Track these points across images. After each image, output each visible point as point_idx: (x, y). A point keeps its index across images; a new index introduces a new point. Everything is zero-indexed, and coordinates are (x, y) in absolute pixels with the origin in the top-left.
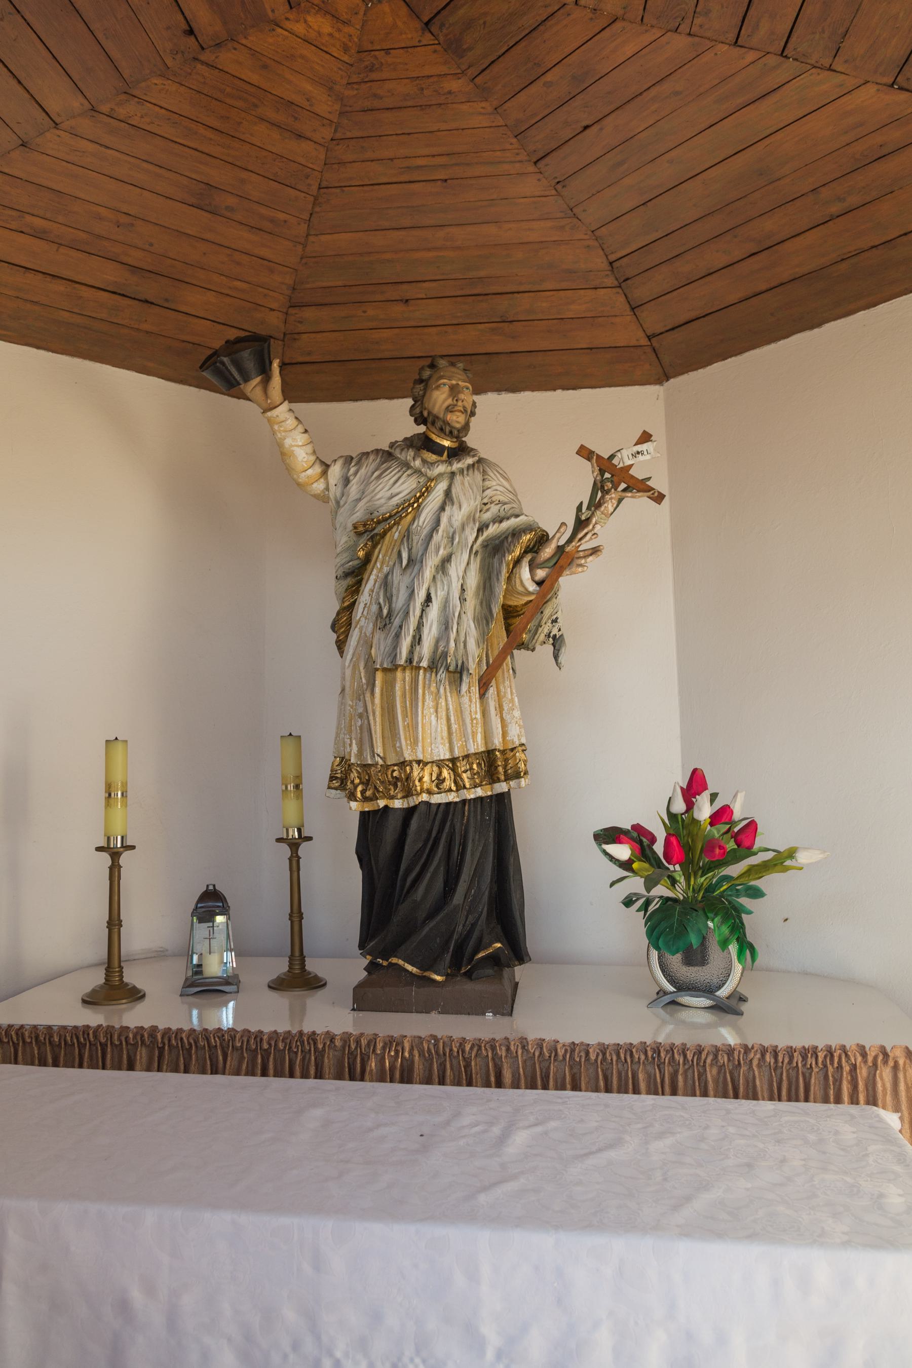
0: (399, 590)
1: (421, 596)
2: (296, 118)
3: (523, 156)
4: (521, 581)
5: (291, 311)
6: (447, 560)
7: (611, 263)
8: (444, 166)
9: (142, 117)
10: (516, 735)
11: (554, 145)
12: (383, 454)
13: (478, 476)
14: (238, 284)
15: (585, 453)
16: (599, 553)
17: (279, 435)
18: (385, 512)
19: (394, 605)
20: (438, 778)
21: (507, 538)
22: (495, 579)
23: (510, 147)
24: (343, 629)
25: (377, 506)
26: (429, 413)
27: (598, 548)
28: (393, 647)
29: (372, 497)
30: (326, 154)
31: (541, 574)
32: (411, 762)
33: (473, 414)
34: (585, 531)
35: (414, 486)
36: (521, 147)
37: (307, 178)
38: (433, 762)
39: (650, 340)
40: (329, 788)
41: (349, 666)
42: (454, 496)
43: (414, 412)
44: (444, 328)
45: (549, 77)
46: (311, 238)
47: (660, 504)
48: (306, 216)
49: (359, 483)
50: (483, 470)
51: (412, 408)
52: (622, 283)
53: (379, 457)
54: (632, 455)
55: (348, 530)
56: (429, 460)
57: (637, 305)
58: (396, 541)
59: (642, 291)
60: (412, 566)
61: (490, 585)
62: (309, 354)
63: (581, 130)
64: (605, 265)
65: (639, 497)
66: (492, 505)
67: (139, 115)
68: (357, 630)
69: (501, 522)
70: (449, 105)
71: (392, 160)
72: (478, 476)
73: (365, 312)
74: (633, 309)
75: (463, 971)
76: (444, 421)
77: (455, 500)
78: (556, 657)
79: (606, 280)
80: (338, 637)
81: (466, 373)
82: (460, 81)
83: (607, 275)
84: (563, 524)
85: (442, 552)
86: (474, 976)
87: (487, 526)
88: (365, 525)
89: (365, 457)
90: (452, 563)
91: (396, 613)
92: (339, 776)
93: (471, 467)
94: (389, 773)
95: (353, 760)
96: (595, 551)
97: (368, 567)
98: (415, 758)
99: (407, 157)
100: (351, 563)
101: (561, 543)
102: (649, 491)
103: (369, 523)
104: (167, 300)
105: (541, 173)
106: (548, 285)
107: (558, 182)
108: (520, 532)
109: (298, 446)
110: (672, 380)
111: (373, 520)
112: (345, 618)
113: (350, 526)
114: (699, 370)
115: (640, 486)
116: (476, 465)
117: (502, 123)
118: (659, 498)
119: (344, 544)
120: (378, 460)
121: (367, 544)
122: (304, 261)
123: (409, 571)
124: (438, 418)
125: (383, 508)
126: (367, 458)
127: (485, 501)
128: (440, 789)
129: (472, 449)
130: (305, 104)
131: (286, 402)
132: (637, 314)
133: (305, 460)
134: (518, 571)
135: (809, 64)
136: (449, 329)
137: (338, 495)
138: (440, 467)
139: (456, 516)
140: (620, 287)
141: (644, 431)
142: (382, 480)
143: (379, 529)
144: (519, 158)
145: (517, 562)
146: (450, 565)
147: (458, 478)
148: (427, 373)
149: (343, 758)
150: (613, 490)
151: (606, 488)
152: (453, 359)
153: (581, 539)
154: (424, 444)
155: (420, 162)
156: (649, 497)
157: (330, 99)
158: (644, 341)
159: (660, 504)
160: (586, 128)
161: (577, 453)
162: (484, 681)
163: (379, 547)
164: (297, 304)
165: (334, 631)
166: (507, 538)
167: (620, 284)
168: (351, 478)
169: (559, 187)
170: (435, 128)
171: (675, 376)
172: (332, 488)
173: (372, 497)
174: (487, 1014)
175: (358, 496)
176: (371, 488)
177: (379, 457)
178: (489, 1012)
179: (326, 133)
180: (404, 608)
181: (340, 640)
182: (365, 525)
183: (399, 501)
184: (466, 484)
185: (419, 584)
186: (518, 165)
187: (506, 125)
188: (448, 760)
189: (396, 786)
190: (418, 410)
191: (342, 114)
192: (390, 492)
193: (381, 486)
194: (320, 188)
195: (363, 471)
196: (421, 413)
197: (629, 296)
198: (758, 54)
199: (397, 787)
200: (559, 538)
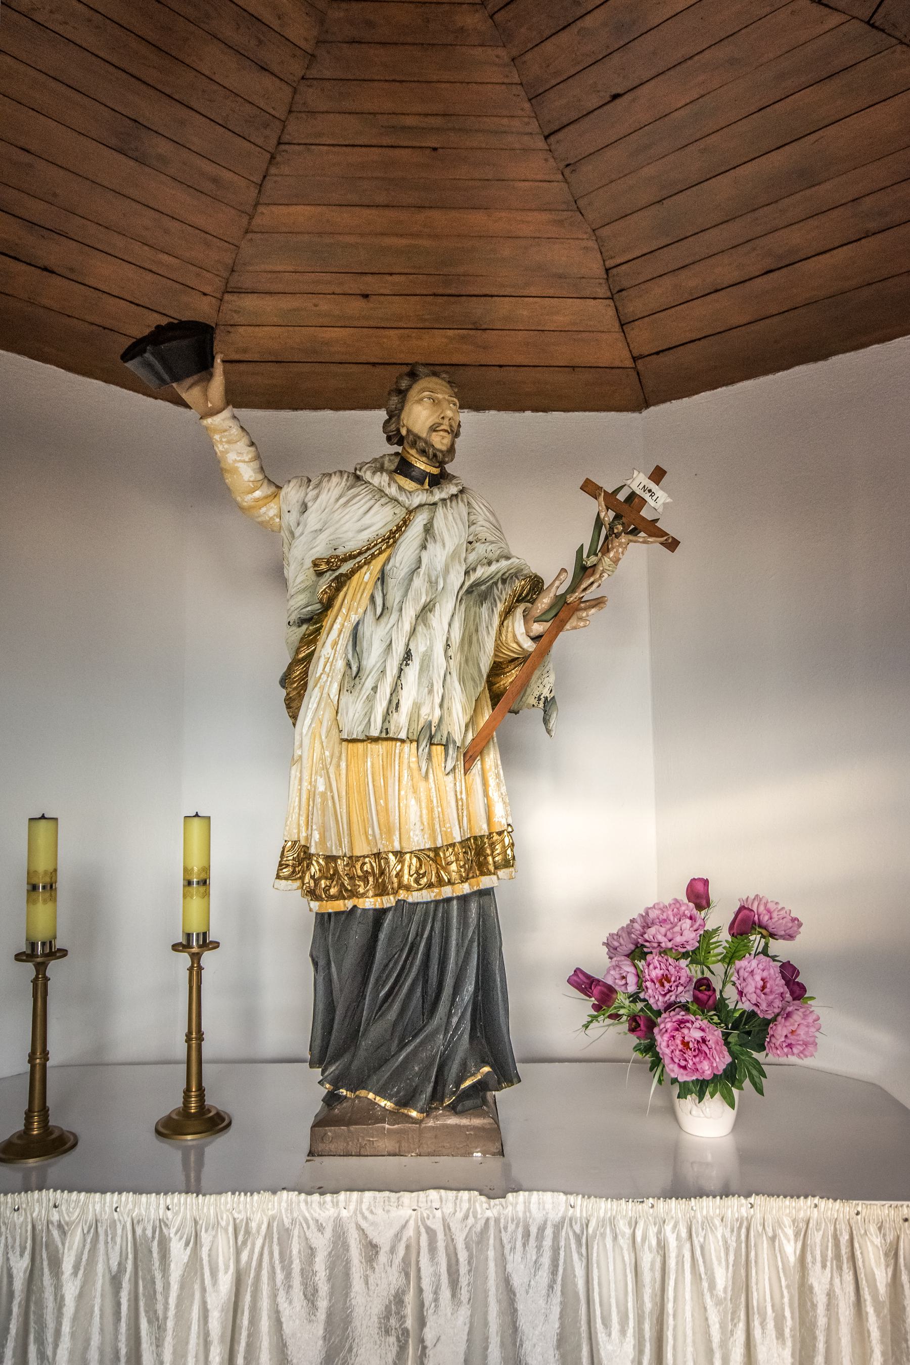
0: (371, 644)
1: (399, 650)
2: (260, 42)
3: (534, 126)
4: (515, 636)
5: (227, 297)
6: (427, 609)
7: (607, 270)
8: (438, 130)
9: (51, 12)
10: (500, 817)
11: (574, 115)
12: (348, 477)
13: (463, 508)
14: (165, 258)
15: (590, 488)
16: (602, 605)
17: (221, 448)
18: (353, 547)
19: (364, 663)
20: (417, 872)
21: (496, 583)
22: (485, 633)
23: (520, 113)
24: (295, 685)
25: (344, 540)
26: (409, 431)
27: (601, 600)
28: (364, 712)
29: (337, 529)
30: (293, 98)
31: (538, 628)
32: (387, 853)
33: (457, 435)
34: (592, 579)
35: (390, 518)
36: (533, 115)
37: (266, 128)
38: (411, 852)
39: (635, 361)
40: (278, 877)
41: (307, 734)
42: (436, 532)
43: (389, 429)
44: (407, 331)
45: (588, 21)
46: (261, 209)
47: (673, 552)
48: (257, 179)
49: (320, 512)
50: (468, 502)
51: (386, 423)
52: (615, 295)
53: (344, 480)
54: (644, 486)
55: (305, 567)
56: (406, 487)
57: (627, 321)
58: (367, 583)
59: (634, 306)
60: (388, 615)
61: (478, 640)
62: (245, 351)
63: (609, 99)
64: (601, 273)
65: (652, 542)
66: (478, 544)
67: (48, 8)
68: (317, 689)
69: (490, 563)
70: (458, 47)
71: (374, 114)
72: (463, 508)
73: (316, 305)
74: (622, 325)
75: (447, 1102)
76: (426, 442)
77: (438, 537)
78: (546, 721)
79: (598, 290)
80: (288, 694)
81: (451, 386)
82: (477, 15)
83: (600, 284)
84: (564, 570)
85: (424, 599)
86: (459, 1108)
87: (474, 570)
88: (328, 562)
89: (326, 479)
90: (436, 613)
91: (367, 672)
92: (290, 863)
93: (454, 497)
94: (358, 866)
95: (313, 850)
96: (598, 602)
97: (329, 612)
98: (390, 848)
99: (394, 113)
100: (309, 608)
101: (561, 591)
102: (662, 537)
103: (333, 560)
104: (72, 270)
105: (550, 151)
106: (533, 291)
107: (568, 165)
108: (512, 577)
109: (244, 462)
110: (652, 408)
111: (337, 556)
112: (298, 673)
113: (308, 563)
114: (684, 399)
115: (652, 529)
116: (460, 495)
117: (516, 79)
118: (672, 545)
119: (300, 584)
120: (343, 484)
121: (330, 586)
122: (249, 236)
123: (384, 620)
124: (419, 438)
125: (351, 543)
126: (329, 481)
127: (471, 539)
128: (420, 885)
129: (454, 477)
130: (275, 24)
131: (230, 407)
132: (625, 331)
133: (252, 479)
134: (510, 624)
135: (896, 38)
136: (414, 333)
137: (293, 524)
138: (420, 497)
139: (436, 555)
140: (612, 299)
141: (657, 466)
142: (348, 510)
143: (345, 568)
144: (528, 129)
145: (508, 612)
146: (434, 616)
147: (440, 511)
148: (404, 384)
149: (295, 842)
150: (623, 534)
151: (616, 531)
152: (435, 369)
153: (585, 589)
154: (404, 468)
155: (409, 121)
156: (662, 544)
157: (308, 19)
158: (629, 363)
159: (673, 552)
160: (616, 97)
161: (581, 488)
162: (470, 754)
163: (345, 589)
164: (235, 290)
165: (283, 687)
166: (496, 583)
167: (612, 295)
168: (309, 504)
169: (567, 171)
170: (435, 78)
171: (654, 405)
172: (286, 516)
173: (337, 529)
174: (475, 1154)
175: (318, 527)
176: (336, 516)
177: (344, 480)
178: (477, 1152)
179: (296, 68)
180: (378, 665)
181: (290, 698)
182: (328, 562)
183: (370, 536)
184: (450, 518)
185: (398, 638)
186: (526, 138)
187: (521, 84)
188: (429, 849)
189: (366, 882)
190: (393, 427)
191: (319, 42)
192: (360, 523)
193: (347, 517)
194: (279, 143)
195: (323, 497)
196: (398, 430)
197: (620, 309)
198: (844, 18)
199: (368, 883)
200: (558, 587)
